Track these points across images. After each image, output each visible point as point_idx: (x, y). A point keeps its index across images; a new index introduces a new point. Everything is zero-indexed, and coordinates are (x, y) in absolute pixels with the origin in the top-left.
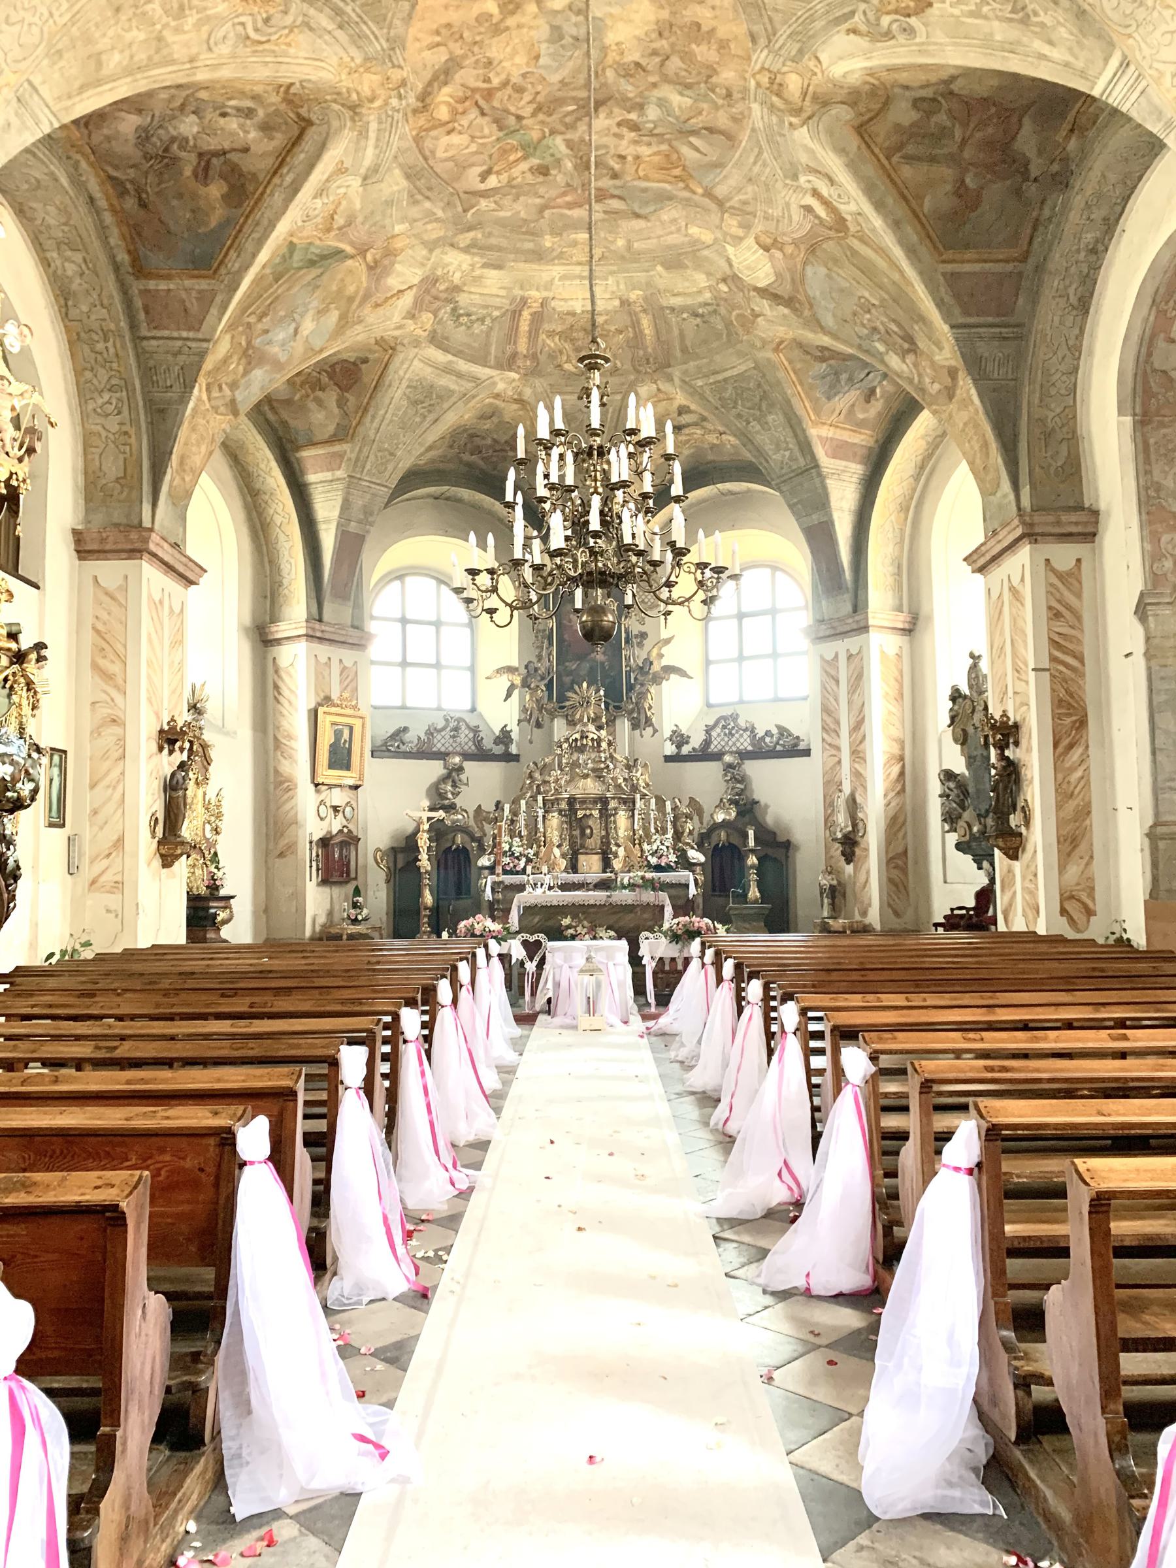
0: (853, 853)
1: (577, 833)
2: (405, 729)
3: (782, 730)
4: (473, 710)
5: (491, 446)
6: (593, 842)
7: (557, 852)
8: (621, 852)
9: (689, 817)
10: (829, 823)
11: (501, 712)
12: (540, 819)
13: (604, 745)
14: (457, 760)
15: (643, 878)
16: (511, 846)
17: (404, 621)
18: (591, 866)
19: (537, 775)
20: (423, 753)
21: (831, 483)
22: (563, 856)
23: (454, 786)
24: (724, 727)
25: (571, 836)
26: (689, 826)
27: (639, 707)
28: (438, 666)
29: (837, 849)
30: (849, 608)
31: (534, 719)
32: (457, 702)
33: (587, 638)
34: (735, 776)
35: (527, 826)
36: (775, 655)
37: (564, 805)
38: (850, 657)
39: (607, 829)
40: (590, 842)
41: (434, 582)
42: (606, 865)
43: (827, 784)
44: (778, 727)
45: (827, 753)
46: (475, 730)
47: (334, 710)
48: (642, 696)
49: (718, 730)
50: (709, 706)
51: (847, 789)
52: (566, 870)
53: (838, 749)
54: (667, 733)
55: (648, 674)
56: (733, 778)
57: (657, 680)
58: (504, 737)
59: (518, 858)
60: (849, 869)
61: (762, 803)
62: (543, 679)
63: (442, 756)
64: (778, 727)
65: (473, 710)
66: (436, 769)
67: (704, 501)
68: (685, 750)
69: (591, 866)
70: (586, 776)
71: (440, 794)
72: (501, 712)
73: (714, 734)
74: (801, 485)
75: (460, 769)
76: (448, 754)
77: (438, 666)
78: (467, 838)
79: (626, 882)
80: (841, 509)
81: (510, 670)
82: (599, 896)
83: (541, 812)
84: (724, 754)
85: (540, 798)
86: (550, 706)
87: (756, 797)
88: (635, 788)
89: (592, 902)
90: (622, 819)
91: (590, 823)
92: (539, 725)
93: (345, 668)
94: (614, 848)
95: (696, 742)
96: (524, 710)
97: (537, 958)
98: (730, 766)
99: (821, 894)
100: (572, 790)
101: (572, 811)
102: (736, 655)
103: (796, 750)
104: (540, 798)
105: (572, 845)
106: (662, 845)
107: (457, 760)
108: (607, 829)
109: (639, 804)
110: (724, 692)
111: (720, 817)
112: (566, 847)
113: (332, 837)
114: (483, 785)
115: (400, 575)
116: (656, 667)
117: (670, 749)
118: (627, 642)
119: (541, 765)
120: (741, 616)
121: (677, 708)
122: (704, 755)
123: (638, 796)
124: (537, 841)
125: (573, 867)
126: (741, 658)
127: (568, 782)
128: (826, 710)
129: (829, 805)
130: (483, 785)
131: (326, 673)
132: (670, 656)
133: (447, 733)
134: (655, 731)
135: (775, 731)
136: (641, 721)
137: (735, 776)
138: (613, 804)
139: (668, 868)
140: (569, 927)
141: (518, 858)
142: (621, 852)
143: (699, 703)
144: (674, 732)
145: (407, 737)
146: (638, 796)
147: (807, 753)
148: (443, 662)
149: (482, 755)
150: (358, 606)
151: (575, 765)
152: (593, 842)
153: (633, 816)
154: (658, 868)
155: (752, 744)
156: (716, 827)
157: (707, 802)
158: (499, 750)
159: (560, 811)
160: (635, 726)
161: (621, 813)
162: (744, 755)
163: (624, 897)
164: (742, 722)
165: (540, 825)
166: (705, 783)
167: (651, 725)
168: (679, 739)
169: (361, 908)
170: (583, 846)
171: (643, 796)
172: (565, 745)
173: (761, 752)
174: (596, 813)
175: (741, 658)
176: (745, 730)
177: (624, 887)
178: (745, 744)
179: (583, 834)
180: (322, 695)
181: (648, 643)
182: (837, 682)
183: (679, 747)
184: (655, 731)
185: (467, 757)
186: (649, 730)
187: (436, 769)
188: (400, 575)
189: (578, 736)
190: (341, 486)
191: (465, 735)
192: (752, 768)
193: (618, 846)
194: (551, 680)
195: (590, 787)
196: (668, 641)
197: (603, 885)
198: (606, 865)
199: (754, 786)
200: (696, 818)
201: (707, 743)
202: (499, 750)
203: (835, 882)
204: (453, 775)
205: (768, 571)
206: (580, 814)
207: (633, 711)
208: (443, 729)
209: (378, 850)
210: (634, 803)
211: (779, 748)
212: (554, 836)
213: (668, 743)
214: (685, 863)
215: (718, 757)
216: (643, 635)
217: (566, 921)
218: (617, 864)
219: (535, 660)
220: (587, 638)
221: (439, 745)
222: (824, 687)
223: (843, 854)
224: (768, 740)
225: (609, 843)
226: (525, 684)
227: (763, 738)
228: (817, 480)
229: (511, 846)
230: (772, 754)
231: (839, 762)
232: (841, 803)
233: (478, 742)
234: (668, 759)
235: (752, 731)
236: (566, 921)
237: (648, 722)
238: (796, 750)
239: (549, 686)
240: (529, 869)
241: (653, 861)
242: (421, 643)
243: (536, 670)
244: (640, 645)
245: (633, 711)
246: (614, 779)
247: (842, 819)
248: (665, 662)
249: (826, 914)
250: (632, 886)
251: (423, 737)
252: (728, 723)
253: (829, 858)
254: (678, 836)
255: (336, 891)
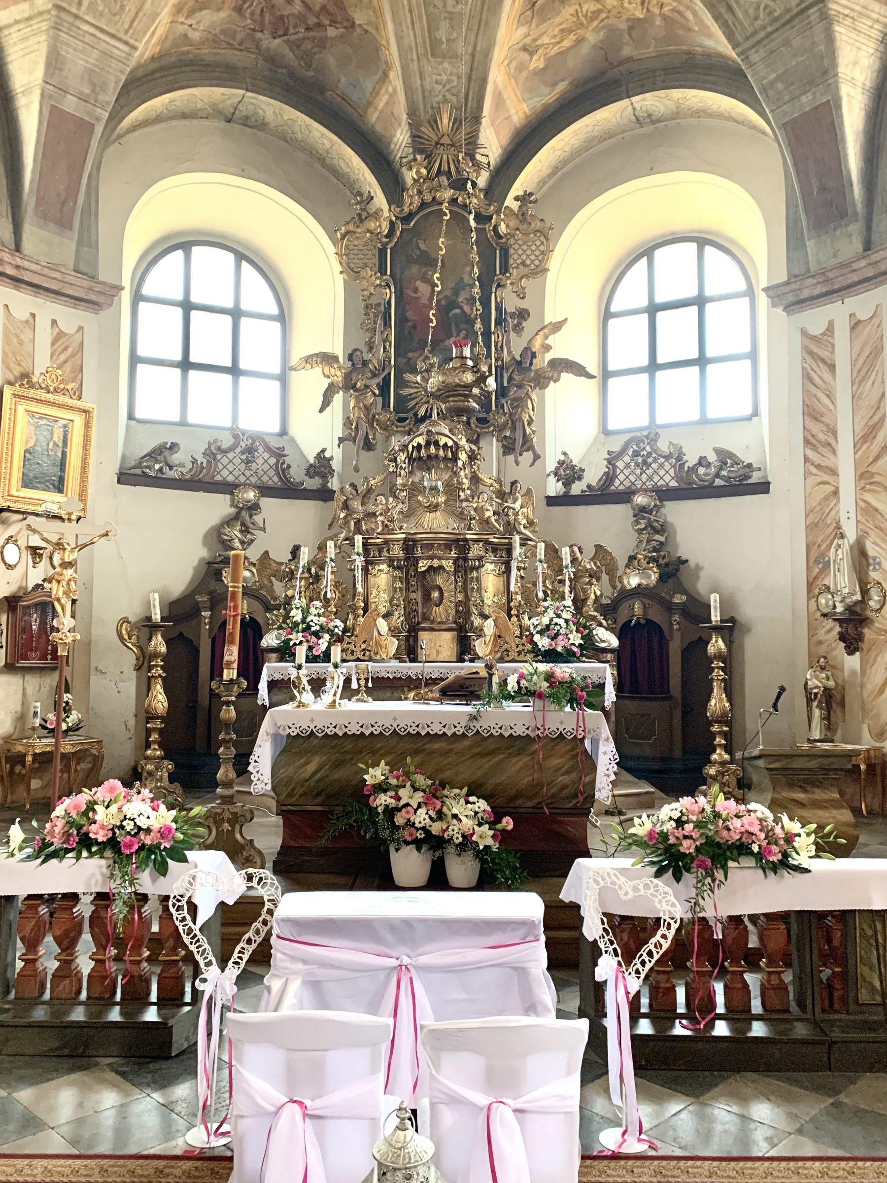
0: (860, 638)
1: (417, 596)
2: (174, 447)
3: (724, 456)
4: (284, 433)
5: (302, 18)
6: (443, 612)
7: (382, 625)
8: (489, 627)
9: (594, 575)
10: (814, 588)
11: (318, 430)
12: (359, 574)
13: (463, 456)
14: (251, 495)
15: (549, 677)
16: (306, 612)
17: (187, 306)
18: (438, 645)
19: (356, 504)
20: (198, 482)
21: (840, 30)
22: (394, 632)
23: (245, 530)
24: (636, 454)
25: (408, 601)
26: (595, 590)
27: (514, 422)
28: (234, 370)
29: (831, 631)
30: (857, 245)
31: (358, 436)
32: (259, 416)
33: (440, 320)
34: (652, 526)
35: (337, 584)
36: (701, 361)
37: (397, 551)
38: (856, 325)
39: (465, 589)
40: (438, 612)
41: (230, 257)
42: (464, 650)
43: (811, 528)
44: (718, 451)
45: (812, 480)
46: (279, 454)
47: (31, 393)
48: (520, 403)
49: (627, 459)
50: (606, 432)
51: (851, 534)
52: (397, 657)
53: (834, 472)
54: (551, 465)
55: (525, 374)
56: (650, 525)
57: (541, 381)
58: (321, 466)
59: (317, 635)
60: (853, 662)
61: (692, 564)
62: (374, 376)
63: (228, 488)
64: (718, 451)
65: (284, 433)
66: (219, 506)
67: (609, 135)
68: (577, 489)
69: (438, 645)
70: (433, 508)
71: (223, 542)
72: (318, 430)
73: (620, 464)
74: (787, 43)
75: (254, 508)
76: (236, 486)
77: (234, 370)
78: (256, 605)
79: (512, 685)
80: (852, 81)
81: (328, 359)
82: (455, 711)
83: (359, 561)
84: (634, 493)
85: (359, 539)
86: (383, 417)
87: (683, 552)
88: (511, 528)
89: (436, 729)
90: (490, 578)
91: (439, 581)
92: (368, 446)
93: (60, 336)
94: (477, 621)
95: (593, 476)
96: (347, 422)
97: (243, 951)
98: (643, 509)
99: (809, 701)
100: (409, 527)
101: (411, 560)
102: (645, 361)
103: (740, 482)
104: (359, 539)
105: (409, 614)
106: (555, 614)
107: (251, 495)
108: (465, 589)
109: (517, 551)
110: (629, 408)
111: (633, 581)
112: (398, 618)
113: (26, 593)
114: (287, 528)
115: (183, 243)
116: (538, 363)
117: (554, 488)
118: (498, 323)
119: (362, 489)
120: (653, 310)
121: (569, 425)
122: (604, 494)
123: (517, 539)
124: (354, 609)
125: (410, 650)
126: (653, 366)
127: (407, 515)
128: (811, 413)
129: (818, 562)
130: (287, 528)
131: (26, 336)
132: (561, 346)
133: (236, 457)
134: (537, 457)
135: (712, 458)
136: (518, 442)
137: (652, 526)
138: (476, 551)
139: (567, 656)
140: (381, 788)
141: (317, 635)
142: (489, 627)
143: (592, 429)
144: (561, 463)
145: (176, 458)
146: (517, 539)
147: (763, 487)
148: (243, 365)
149: (288, 490)
150: (88, 240)
151: (415, 489)
152: (443, 612)
153: (508, 571)
154: (551, 656)
155: (678, 478)
156: (627, 595)
157: (620, 553)
158: (313, 483)
159: (391, 562)
160: (508, 448)
161: (490, 567)
162: (665, 494)
163: (514, 717)
164: (663, 446)
165: (360, 589)
166: (609, 529)
167: (531, 448)
168: (568, 473)
169: (67, 710)
170: (426, 618)
171: (524, 541)
172: (402, 457)
173: (692, 488)
174: (448, 565)
175: (653, 366)
176: (667, 458)
177: (509, 697)
178: (668, 478)
179: (427, 597)
180: (17, 371)
181: (529, 326)
182: (832, 368)
183: (567, 484)
184: (537, 457)
185: (266, 491)
186: (528, 456)
187: (219, 506)
188: (183, 243)
189: (421, 440)
190: (45, 26)
191: (263, 462)
192: (677, 513)
193: (485, 617)
194: (387, 380)
195: (437, 523)
196: (557, 327)
197: (461, 690)
198: (464, 650)
199: (678, 539)
200: (605, 578)
201: (609, 477)
202: (311, 485)
203: (831, 684)
204: (244, 517)
205: (693, 246)
206: (423, 565)
207: (503, 427)
208: (232, 449)
209: (125, 620)
210: (509, 549)
211: (718, 482)
212: (381, 599)
213: (552, 479)
214: (590, 649)
215: (624, 497)
216: (523, 314)
217: (375, 775)
218: (481, 647)
219: (365, 349)
220: (440, 320)
221: (227, 471)
222: (807, 377)
223: (842, 637)
224: (701, 471)
225: (468, 613)
226: (349, 385)
227: (693, 469)
228: (818, 29)
229: (306, 612)
230: (708, 491)
231: (836, 493)
232: (841, 556)
233: (282, 471)
234: (552, 501)
235: (679, 459)
236: (375, 775)
237: (527, 444)
238: (740, 482)
239: (384, 388)
240: (336, 653)
241: (543, 643)
242: (211, 340)
243: (365, 363)
244: (518, 329)
245: (503, 427)
246: (479, 510)
247: (843, 581)
248: (554, 354)
249: (816, 734)
250: (523, 694)
251: (200, 459)
252: (641, 447)
253: (814, 642)
254: (579, 604)
255: (33, 682)
